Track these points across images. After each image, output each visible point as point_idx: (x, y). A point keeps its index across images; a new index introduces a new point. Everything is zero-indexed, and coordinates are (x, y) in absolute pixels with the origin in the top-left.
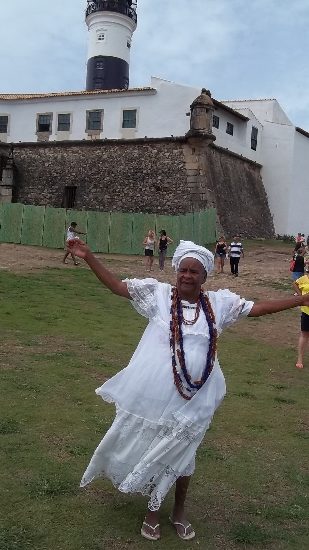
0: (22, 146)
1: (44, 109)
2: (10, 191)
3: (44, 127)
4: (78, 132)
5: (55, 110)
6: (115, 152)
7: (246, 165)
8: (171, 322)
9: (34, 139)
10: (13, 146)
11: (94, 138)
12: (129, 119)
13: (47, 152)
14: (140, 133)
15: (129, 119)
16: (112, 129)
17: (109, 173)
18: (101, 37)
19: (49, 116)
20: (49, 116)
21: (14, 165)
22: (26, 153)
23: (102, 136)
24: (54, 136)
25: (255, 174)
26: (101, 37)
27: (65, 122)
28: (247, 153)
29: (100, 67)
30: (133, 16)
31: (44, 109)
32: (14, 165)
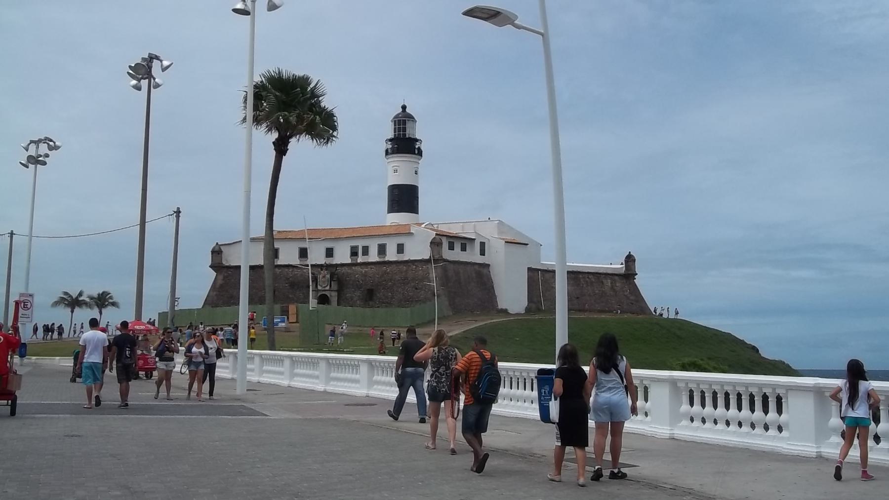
0: (343, 265)
1: (354, 243)
2: (336, 294)
3: (354, 253)
4: (373, 257)
5: (360, 244)
6: (394, 267)
7: (476, 267)
8: (755, 350)
9: (349, 261)
10: (337, 265)
11: (382, 260)
12: (400, 249)
13: (358, 268)
14: (406, 257)
15: (400, 249)
16: (392, 255)
17: (391, 280)
18: (395, 171)
19: (357, 247)
20: (357, 247)
21: (338, 278)
22: (345, 270)
23: (387, 259)
24: (360, 259)
25: (485, 271)
26: (395, 171)
27: (366, 251)
28: (478, 259)
29: (396, 192)
30: (420, 153)
31: (354, 243)
32: (338, 278)
